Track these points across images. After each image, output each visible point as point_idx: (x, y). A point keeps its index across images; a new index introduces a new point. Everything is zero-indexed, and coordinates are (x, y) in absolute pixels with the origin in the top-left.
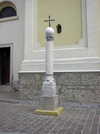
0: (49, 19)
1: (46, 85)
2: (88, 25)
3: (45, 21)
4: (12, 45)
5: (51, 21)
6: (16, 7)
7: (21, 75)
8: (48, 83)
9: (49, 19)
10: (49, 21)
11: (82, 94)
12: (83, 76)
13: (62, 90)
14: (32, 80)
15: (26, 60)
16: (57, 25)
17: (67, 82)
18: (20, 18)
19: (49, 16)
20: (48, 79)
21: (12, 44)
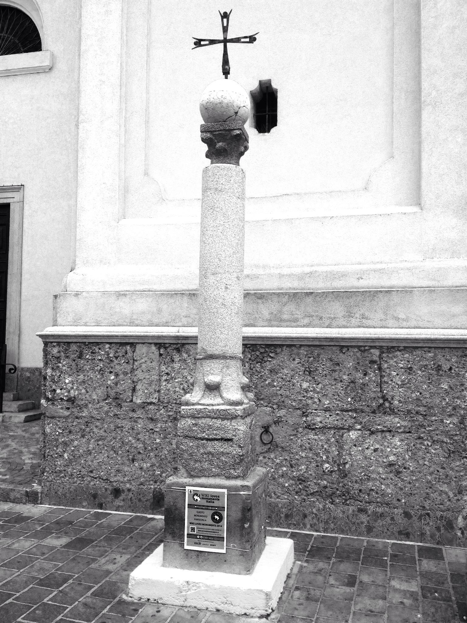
0: (225, 30)
1: (199, 411)
2: (425, 85)
3: (198, 43)
4: (17, 196)
5: (232, 41)
6: (37, 10)
7: (58, 346)
8: (213, 402)
9: (225, 30)
10: (225, 41)
11: (392, 458)
12: (401, 360)
13: (280, 434)
14: (117, 375)
15: (188, 511)
16: (254, 86)
17: (307, 391)
18: (61, 66)
19: (225, 16)
20: (213, 379)
21: (20, 188)
